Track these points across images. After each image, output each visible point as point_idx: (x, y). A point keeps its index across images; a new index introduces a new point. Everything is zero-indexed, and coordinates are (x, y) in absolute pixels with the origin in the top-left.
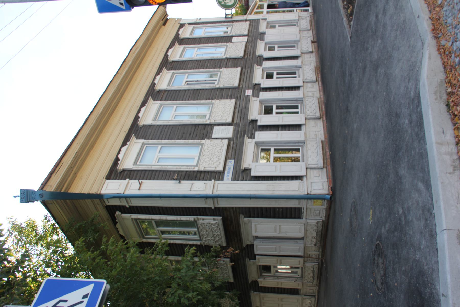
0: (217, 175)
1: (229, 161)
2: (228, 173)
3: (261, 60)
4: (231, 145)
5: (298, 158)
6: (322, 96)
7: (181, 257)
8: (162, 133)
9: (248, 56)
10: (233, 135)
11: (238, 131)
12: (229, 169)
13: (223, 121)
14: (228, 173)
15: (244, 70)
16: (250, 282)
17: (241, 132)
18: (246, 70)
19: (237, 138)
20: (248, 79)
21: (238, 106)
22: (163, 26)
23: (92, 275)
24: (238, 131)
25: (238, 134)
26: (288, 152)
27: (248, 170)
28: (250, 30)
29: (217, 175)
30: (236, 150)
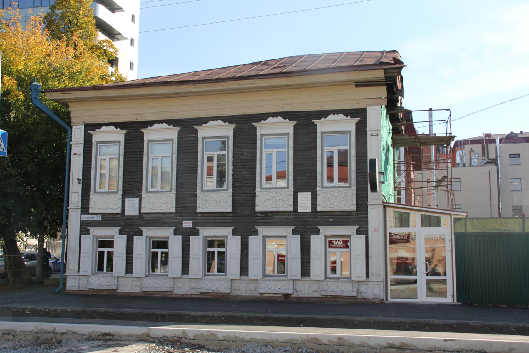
0: (85, 208)
1: (101, 216)
2: (88, 218)
3: (186, 236)
4: (116, 216)
5: (102, 270)
6: (175, 296)
7: (402, 191)
8: (130, 153)
9: (259, 217)
10: (128, 216)
11: (133, 219)
12: (92, 218)
13: (143, 206)
14: (88, 218)
15: (231, 215)
16: (257, 227)
17: (132, 222)
18: (230, 218)
19: (125, 219)
20: (211, 221)
21: (166, 216)
22: (354, 86)
23: (451, 162)
24: (133, 219)
25: (129, 219)
26: (104, 262)
27: (87, 232)
28: (332, 214)
29: (85, 208)
30: (111, 220)
